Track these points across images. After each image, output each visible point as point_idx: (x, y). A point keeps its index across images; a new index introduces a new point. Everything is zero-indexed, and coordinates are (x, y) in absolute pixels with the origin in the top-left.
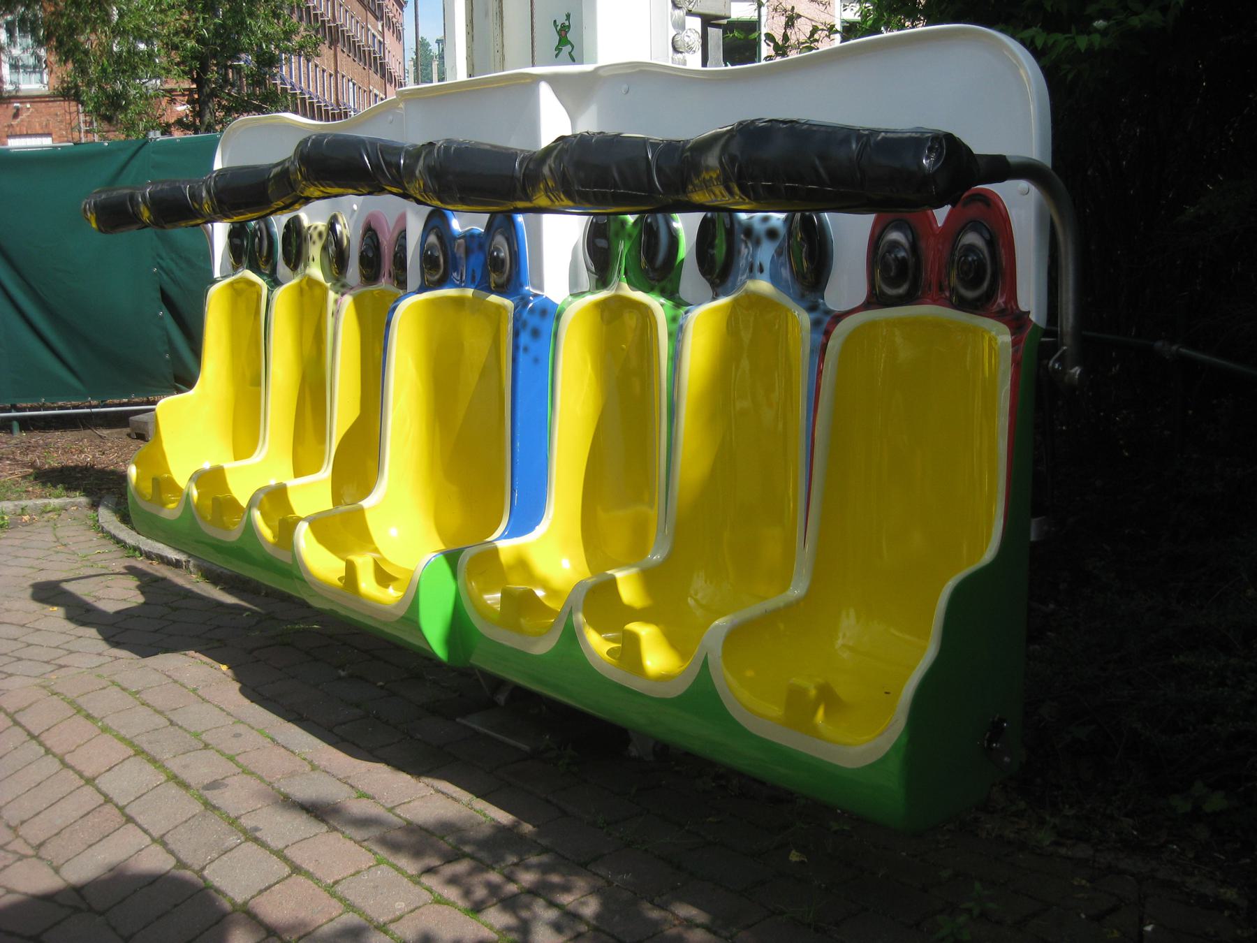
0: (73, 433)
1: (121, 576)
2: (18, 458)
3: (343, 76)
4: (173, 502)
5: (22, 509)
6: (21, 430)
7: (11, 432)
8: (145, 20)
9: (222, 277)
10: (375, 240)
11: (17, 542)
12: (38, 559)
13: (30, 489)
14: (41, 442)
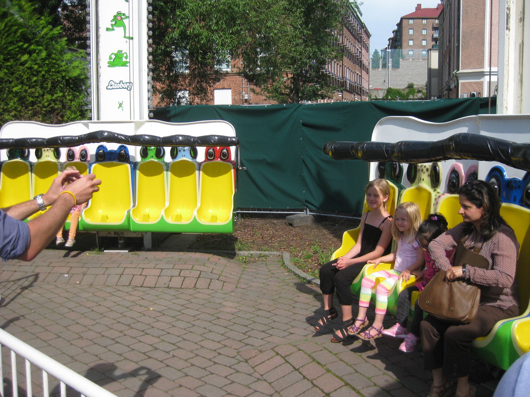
3: (345, 66)
10: (457, 175)
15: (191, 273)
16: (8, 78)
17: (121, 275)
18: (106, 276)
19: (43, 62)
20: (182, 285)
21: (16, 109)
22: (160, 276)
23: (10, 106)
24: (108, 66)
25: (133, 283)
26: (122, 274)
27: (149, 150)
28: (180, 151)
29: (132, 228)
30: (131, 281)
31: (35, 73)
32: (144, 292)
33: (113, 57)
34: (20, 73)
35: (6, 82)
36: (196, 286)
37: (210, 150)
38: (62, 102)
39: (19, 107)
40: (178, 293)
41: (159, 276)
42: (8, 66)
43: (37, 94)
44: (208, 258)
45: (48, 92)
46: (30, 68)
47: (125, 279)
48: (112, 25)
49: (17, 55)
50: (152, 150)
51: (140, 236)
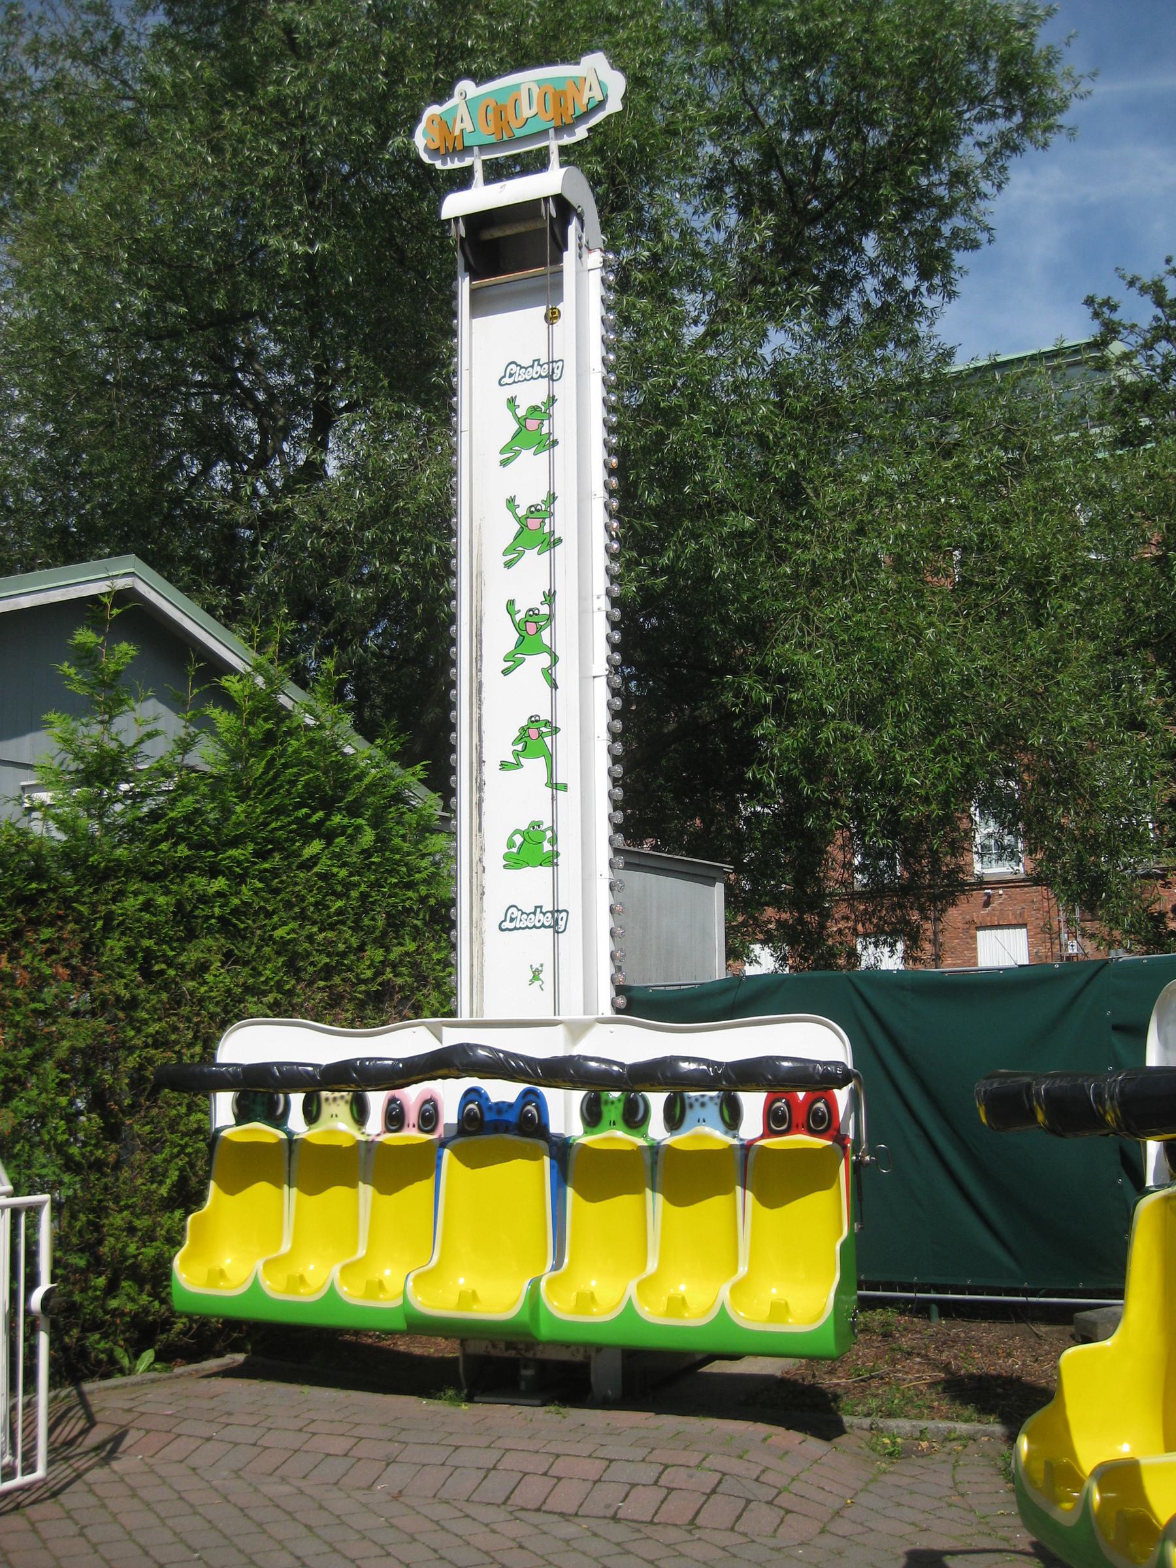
0: (1003, 1326)
1: (1024, 1558)
2: (931, 1355)
4: (1070, 1499)
5: (921, 1432)
6: (940, 1316)
7: (929, 1318)
8: (1123, 796)
9: (1156, 1186)
11: (905, 1481)
12: (924, 1512)
13: (936, 1404)
14: (962, 1335)
15: (691, 1476)
16: (262, 904)
17: (489, 1470)
18: (446, 1471)
19: (366, 858)
20: (656, 1513)
21: (279, 986)
22: (599, 1480)
23: (263, 979)
24: (505, 866)
25: (517, 1499)
26: (494, 1468)
27: (606, 1102)
28: (691, 1106)
29: (545, 1332)
30: (512, 1492)
31: (339, 888)
32: (536, 1526)
33: (518, 839)
34: (297, 888)
35: (256, 913)
36: (698, 1521)
37: (778, 1104)
38: (415, 965)
39: (288, 982)
40: (638, 1535)
41: (595, 1482)
42: (266, 870)
43: (341, 947)
44: (763, 1436)
45: (375, 941)
46: (323, 877)
47: (497, 1486)
48: (516, 754)
49: (294, 841)
50: (613, 1103)
51: (579, 1358)
